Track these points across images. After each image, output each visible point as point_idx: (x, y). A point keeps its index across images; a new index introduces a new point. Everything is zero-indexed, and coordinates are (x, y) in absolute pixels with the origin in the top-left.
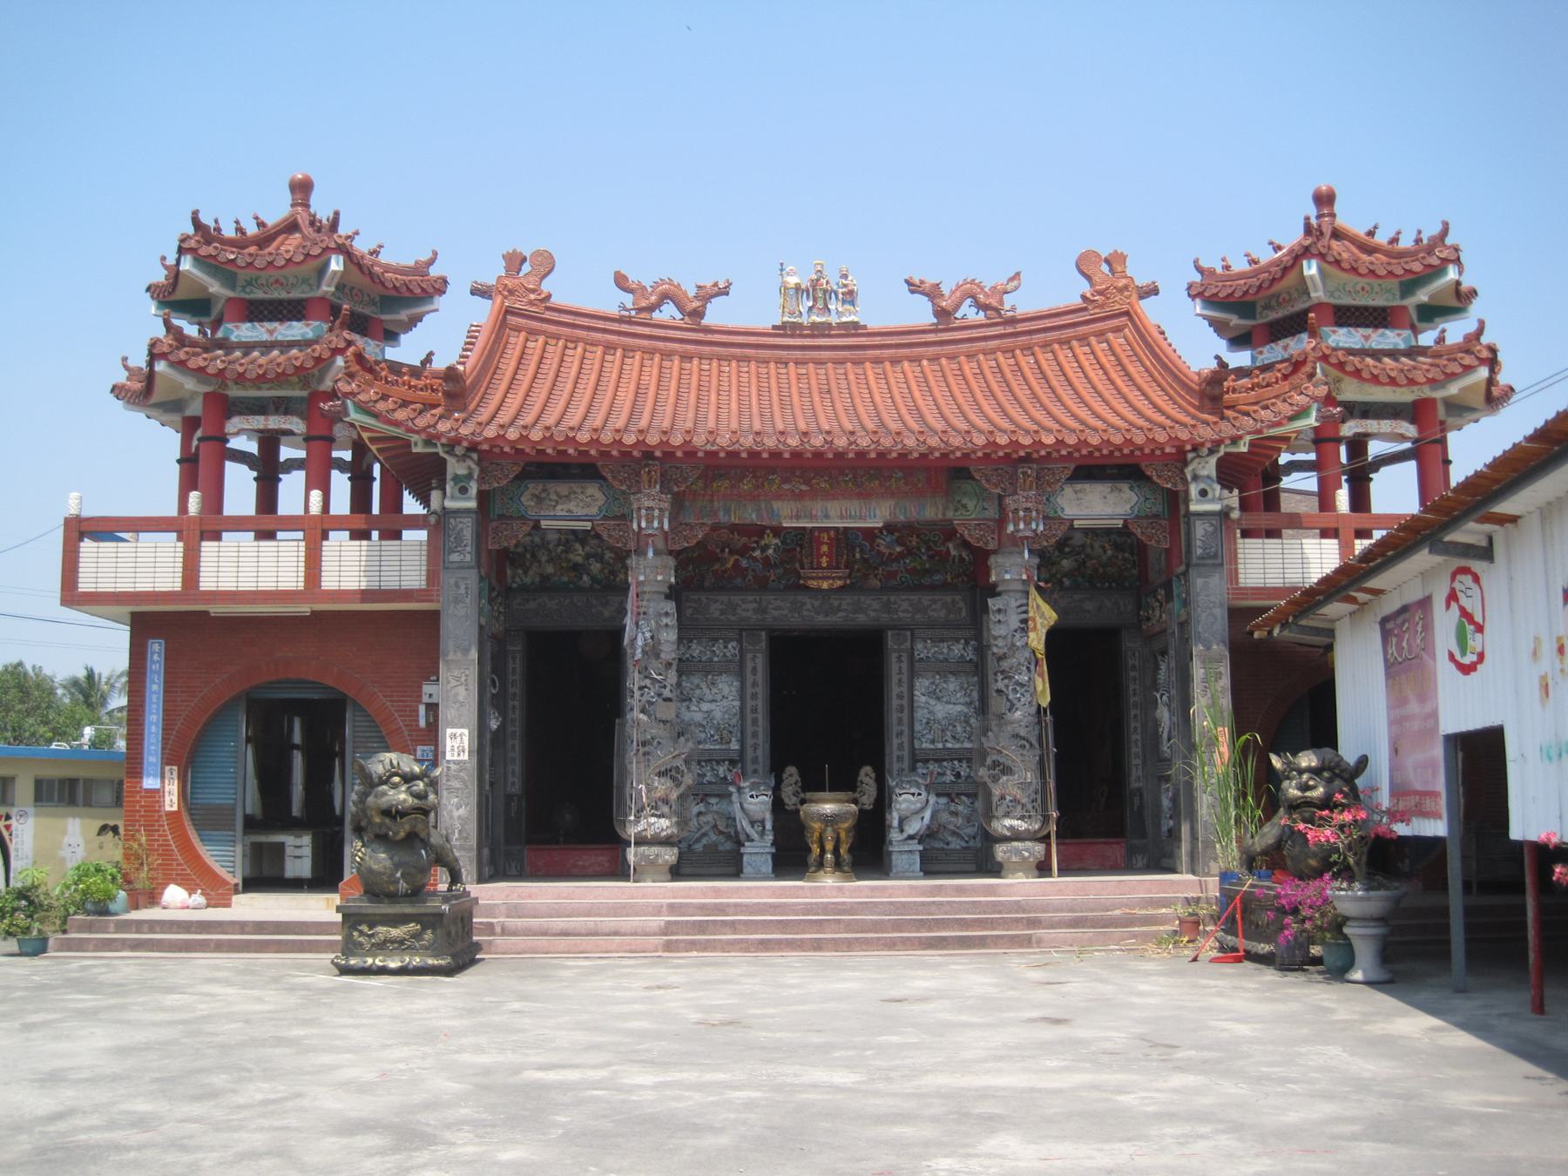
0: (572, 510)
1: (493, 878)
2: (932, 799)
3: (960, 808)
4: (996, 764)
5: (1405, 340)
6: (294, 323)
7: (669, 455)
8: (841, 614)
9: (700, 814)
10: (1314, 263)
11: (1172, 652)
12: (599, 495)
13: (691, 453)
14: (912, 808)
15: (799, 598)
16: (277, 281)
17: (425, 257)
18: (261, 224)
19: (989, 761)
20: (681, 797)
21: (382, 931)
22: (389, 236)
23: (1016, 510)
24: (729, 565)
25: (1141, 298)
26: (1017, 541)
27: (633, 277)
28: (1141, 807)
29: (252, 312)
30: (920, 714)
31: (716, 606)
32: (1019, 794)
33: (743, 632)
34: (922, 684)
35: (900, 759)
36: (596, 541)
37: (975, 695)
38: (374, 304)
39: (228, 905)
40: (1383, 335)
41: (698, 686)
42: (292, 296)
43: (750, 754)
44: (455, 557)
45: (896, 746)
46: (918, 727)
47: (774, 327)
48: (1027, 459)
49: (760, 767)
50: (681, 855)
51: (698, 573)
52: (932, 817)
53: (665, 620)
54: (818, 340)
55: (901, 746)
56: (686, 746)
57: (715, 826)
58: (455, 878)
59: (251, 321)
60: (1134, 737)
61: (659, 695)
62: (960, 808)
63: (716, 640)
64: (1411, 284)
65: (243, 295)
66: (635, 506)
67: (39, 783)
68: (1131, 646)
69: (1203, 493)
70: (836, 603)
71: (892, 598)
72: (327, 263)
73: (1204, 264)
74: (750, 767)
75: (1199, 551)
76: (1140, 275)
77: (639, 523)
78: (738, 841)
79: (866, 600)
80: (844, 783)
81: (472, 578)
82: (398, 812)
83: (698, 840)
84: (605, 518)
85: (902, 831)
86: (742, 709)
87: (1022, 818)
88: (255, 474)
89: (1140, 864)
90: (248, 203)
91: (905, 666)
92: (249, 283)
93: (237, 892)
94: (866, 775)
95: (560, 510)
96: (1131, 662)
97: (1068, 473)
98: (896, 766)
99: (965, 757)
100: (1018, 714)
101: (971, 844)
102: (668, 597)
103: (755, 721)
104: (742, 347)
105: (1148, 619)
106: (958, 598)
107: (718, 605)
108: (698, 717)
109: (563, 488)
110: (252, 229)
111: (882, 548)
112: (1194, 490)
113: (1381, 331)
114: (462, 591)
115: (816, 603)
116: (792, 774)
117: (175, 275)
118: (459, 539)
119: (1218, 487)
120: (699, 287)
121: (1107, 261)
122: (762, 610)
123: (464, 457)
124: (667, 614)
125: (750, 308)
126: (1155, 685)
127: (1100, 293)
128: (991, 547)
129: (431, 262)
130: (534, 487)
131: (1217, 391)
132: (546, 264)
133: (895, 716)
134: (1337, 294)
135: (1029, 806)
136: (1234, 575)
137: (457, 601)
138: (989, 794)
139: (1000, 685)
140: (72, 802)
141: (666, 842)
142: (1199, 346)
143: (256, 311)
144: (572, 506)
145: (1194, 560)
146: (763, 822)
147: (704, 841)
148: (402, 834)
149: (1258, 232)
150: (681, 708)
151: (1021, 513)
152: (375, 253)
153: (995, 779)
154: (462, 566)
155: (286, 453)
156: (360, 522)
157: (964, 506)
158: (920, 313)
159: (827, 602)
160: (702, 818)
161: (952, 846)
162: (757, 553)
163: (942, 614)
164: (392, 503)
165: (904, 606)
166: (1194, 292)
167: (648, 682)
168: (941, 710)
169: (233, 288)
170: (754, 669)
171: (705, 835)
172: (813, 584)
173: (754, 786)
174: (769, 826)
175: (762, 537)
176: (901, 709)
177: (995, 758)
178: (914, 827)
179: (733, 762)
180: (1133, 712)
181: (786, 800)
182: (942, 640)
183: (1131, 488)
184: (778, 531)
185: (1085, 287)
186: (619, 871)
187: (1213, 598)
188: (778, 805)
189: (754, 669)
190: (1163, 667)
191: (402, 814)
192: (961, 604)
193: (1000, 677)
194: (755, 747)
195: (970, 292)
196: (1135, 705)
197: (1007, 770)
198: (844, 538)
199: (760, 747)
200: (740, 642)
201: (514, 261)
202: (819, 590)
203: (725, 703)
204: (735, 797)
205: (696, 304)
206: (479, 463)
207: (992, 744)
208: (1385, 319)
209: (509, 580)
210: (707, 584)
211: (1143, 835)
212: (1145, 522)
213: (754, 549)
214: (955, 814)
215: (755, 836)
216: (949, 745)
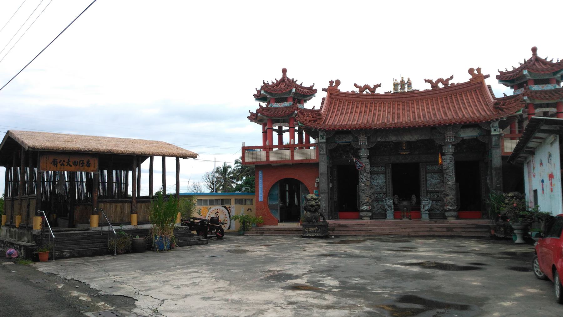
0: (346, 141)
1: (331, 219)
4: (445, 194)
10: (526, 71)
13: (371, 129)
18: (277, 81)
20: (372, 201)
21: (310, 229)
22: (303, 80)
27: (358, 85)
30: (428, 182)
32: (451, 201)
34: (429, 176)
43: (388, 192)
44: (321, 152)
50: (372, 214)
54: (403, 96)
55: (424, 190)
58: (324, 219)
64: (555, 73)
67: (235, 200)
69: (495, 130)
72: (292, 90)
73: (500, 70)
74: (388, 195)
76: (484, 73)
78: (386, 211)
80: (409, 199)
81: (325, 156)
87: (451, 206)
90: (274, 77)
94: (414, 197)
95: (343, 141)
108: (376, 184)
110: (275, 82)
112: (492, 129)
117: (259, 92)
118: (322, 148)
125: (386, 88)
129: (313, 86)
132: (338, 82)
133: (422, 182)
136: (503, 149)
137: (322, 161)
138: (443, 201)
140: (242, 204)
141: (369, 211)
142: (501, 91)
149: (512, 62)
150: (372, 183)
153: (445, 197)
154: (323, 154)
155: (284, 128)
156: (300, 145)
158: (429, 87)
164: (308, 140)
168: (434, 181)
172: (402, 153)
176: (424, 181)
178: (427, 208)
184: (392, 142)
185: (471, 77)
186: (360, 218)
188: (394, 203)
191: (314, 206)
195: (440, 80)
197: (448, 195)
198: (409, 143)
199: (390, 191)
214: (438, 205)
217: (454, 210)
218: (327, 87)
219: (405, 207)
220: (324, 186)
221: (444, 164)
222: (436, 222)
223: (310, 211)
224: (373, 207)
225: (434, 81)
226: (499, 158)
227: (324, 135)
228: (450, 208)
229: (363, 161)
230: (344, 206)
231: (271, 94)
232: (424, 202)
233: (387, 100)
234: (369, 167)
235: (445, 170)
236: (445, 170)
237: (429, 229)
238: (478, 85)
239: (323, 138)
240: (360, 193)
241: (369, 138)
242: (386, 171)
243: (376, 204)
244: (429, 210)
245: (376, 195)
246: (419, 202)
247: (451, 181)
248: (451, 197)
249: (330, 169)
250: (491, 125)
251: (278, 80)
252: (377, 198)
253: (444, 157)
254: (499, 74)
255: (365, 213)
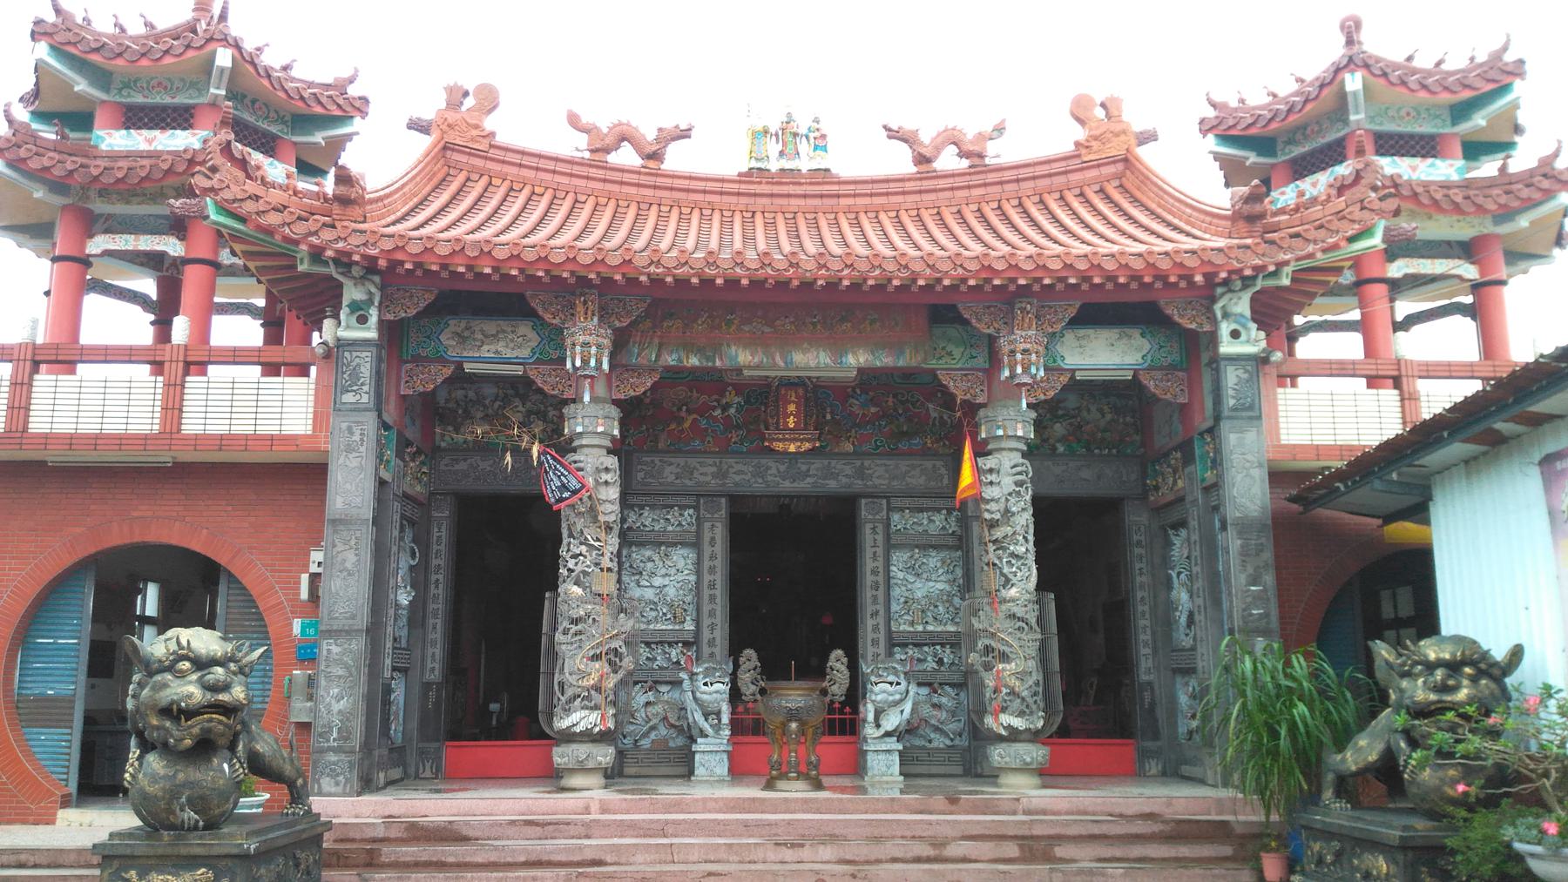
0: (499, 351)
2: (913, 689)
3: (944, 700)
4: (988, 650)
5: (1458, 171)
6: (178, 132)
7: (607, 282)
8: (809, 480)
9: (648, 704)
10: (1359, 75)
11: (1193, 523)
12: (532, 335)
14: (891, 699)
15: (764, 461)
16: (159, 84)
17: (346, 74)
19: (980, 645)
20: (622, 683)
22: (299, 51)
23: (1013, 352)
24: (687, 425)
25: (1140, 144)
26: (1013, 388)
27: (586, 119)
28: (1153, 704)
29: (128, 119)
30: (896, 592)
31: (670, 472)
32: (1014, 682)
33: (699, 498)
34: (899, 558)
35: (875, 642)
36: (539, 397)
37: (959, 572)
38: (285, 123)
39: (50, 821)
40: (1432, 165)
41: (650, 560)
42: (176, 100)
43: (706, 635)
44: (349, 398)
45: (870, 630)
46: (894, 607)
47: (740, 175)
48: (1024, 291)
49: (717, 650)
50: (621, 754)
51: (644, 427)
52: (913, 710)
53: (605, 477)
55: (876, 628)
56: (627, 624)
57: (665, 718)
59: (128, 128)
60: (1142, 623)
61: (597, 564)
62: (944, 700)
63: (672, 507)
64: (1461, 111)
65: (118, 99)
66: (568, 342)
68: (1137, 520)
69: (1235, 334)
70: (804, 468)
71: (867, 463)
72: (211, 59)
73: (1217, 98)
74: (706, 650)
75: (1232, 402)
76: (1136, 121)
77: (573, 361)
78: (690, 735)
79: (838, 465)
80: (815, 670)
81: (370, 422)
82: (180, 711)
83: (646, 735)
84: (538, 362)
85: (878, 726)
86: (698, 583)
87: (1021, 714)
88: (152, 317)
89: (1154, 771)
91: (880, 538)
92: (127, 86)
93: (66, 803)
94: (837, 660)
95: (486, 351)
96: (1135, 538)
97: (1072, 312)
98: (870, 650)
99: (953, 642)
100: (1013, 592)
101: (957, 742)
102: (610, 452)
103: (712, 598)
104: (700, 195)
105: (1157, 488)
106: (939, 463)
107: (672, 468)
108: (649, 594)
109: (490, 326)
111: (855, 409)
112: (1225, 328)
113: (1430, 161)
114: (357, 437)
115: (782, 468)
116: (750, 657)
118: (355, 375)
119: (1254, 326)
120: (660, 130)
121: (1103, 105)
122: (722, 474)
123: (362, 279)
124: (607, 470)
125: (716, 153)
126: (1166, 562)
127: (1096, 138)
128: (980, 400)
129: (351, 81)
130: (456, 325)
131: (1258, 208)
132: (489, 100)
134: (1378, 120)
135: (1030, 700)
137: (349, 449)
138: (982, 685)
139: (992, 557)
141: (603, 737)
143: (135, 118)
144: (500, 347)
145: (1226, 413)
146: (718, 714)
147: (653, 735)
148: (188, 742)
150: (629, 593)
151: (1019, 356)
152: (285, 68)
153: (988, 667)
154: (356, 408)
157: (950, 354)
158: (899, 162)
159: (791, 465)
160: (650, 709)
161: (935, 744)
162: (718, 412)
163: (922, 480)
165: (879, 473)
166: (1206, 127)
167: (583, 548)
168: (921, 589)
169: (107, 90)
170: (713, 539)
171: (653, 728)
172: (779, 446)
173: (707, 673)
174: (725, 719)
175: (722, 395)
177: (987, 642)
178: (892, 721)
179: (686, 644)
180: (1139, 595)
181: (743, 689)
182: (921, 510)
183: (1143, 335)
186: (551, 776)
187: (1249, 457)
188: (735, 695)
189: (713, 539)
190: (1177, 542)
191: (190, 714)
192: (943, 471)
193: (991, 547)
194: (712, 627)
196: (1142, 587)
197: (1004, 657)
199: (717, 631)
200: (696, 508)
201: (456, 96)
202: (786, 453)
203: (680, 577)
204: (686, 684)
205: (654, 148)
206: (382, 288)
207: (985, 625)
208: (1433, 148)
209: (438, 438)
210: (661, 446)
211: (1156, 736)
212: (1159, 375)
213: (714, 408)
215: (710, 731)
216: (930, 628)
217: (1034, 736)
218: (428, 115)
219: (792, 715)
220: (348, 592)
221: (989, 492)
222: (953, 801)
223: (165, 749)
224: (624, 713)
225: (926, 137)
226: (1256, 473)
227: (370, 302)
228: (1018, 723)
229: (588, 468)
230: (494, 707)
231: (101, 77)
232: (879, 692)
233: (716, 198)
234: (613, 493)
235: (993, 525)
236: (993, 525)
237: (926, 850)
238: (1111, 169)
239: (362, 320)
240: (559, 637)
241: (620, 343)
242: (699, 534)
243: (640, 698)
244: (905, 732)
245: (644, 652)
246: (855, 694)
247: (1019, 582)
248: (1017, 667)
249: (402, 513)
250: (1217, 308)
251: (162, 24)
252: (646, 668)
253: (988, 462)
254: (1211, 113)
255: (581, 750)
